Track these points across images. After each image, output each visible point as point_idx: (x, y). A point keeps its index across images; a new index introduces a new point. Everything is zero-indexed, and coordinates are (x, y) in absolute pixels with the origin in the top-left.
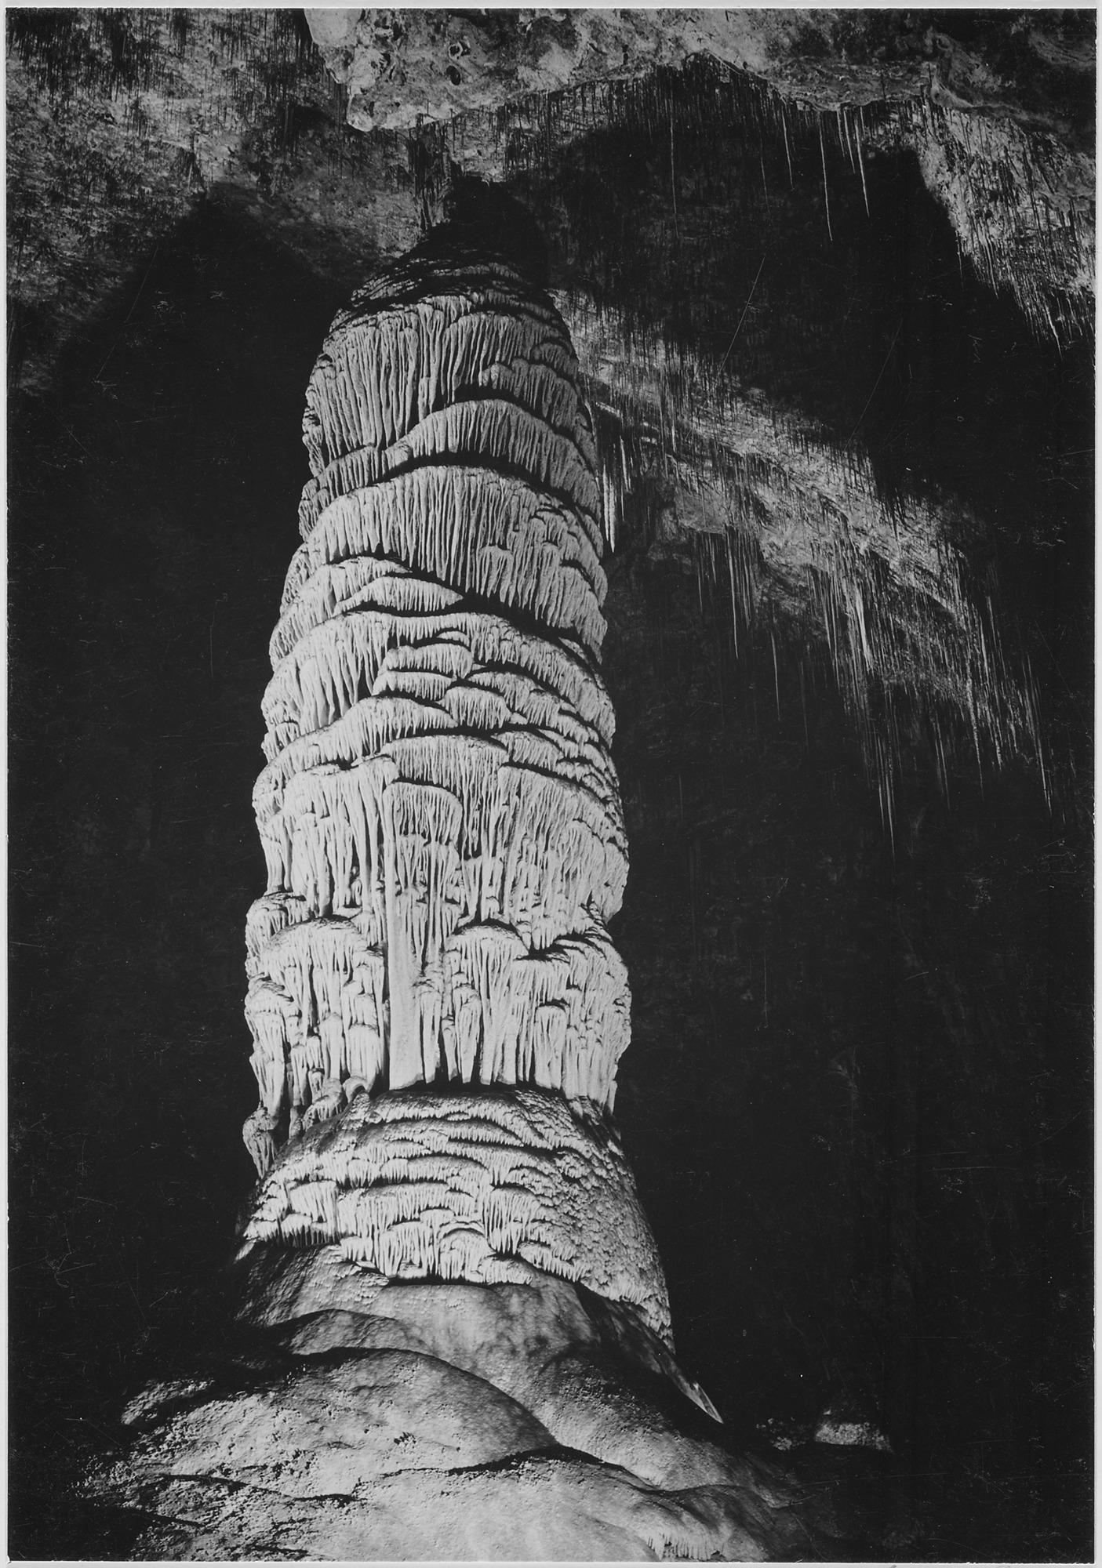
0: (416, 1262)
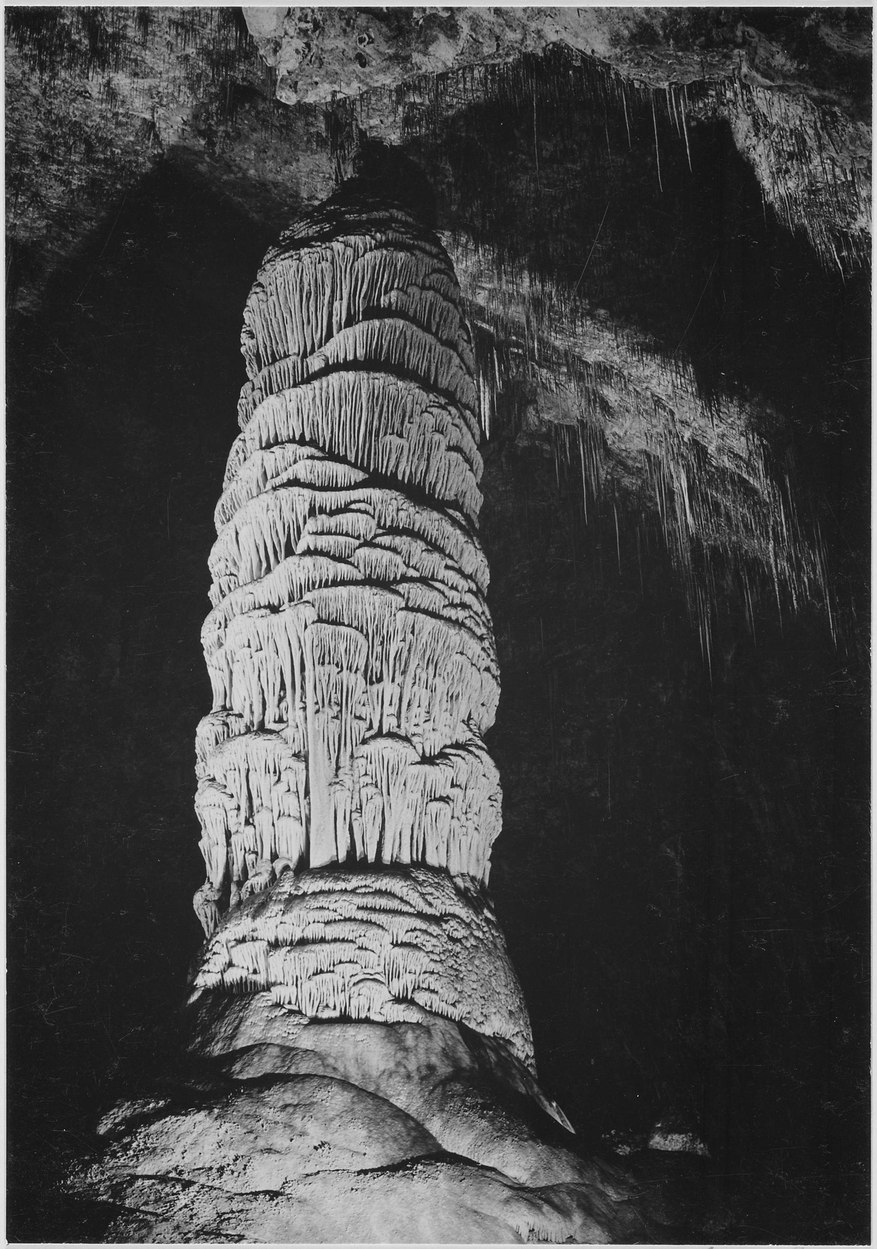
0: (331, 1005)
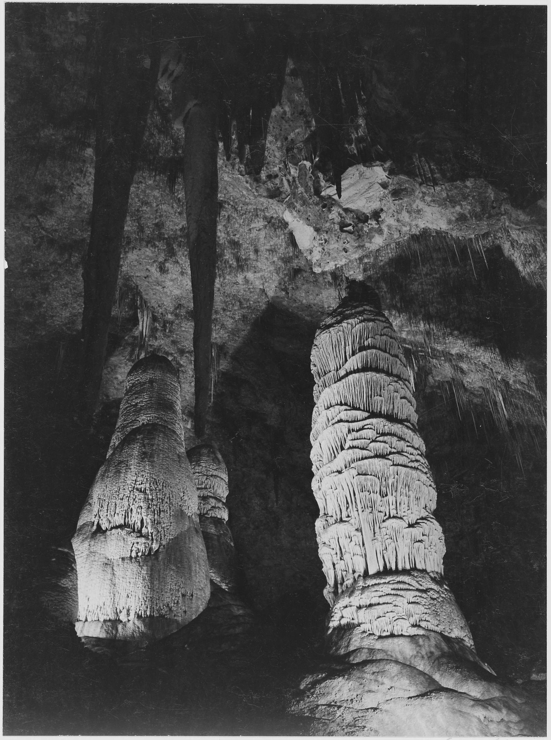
0: (386, 630)
